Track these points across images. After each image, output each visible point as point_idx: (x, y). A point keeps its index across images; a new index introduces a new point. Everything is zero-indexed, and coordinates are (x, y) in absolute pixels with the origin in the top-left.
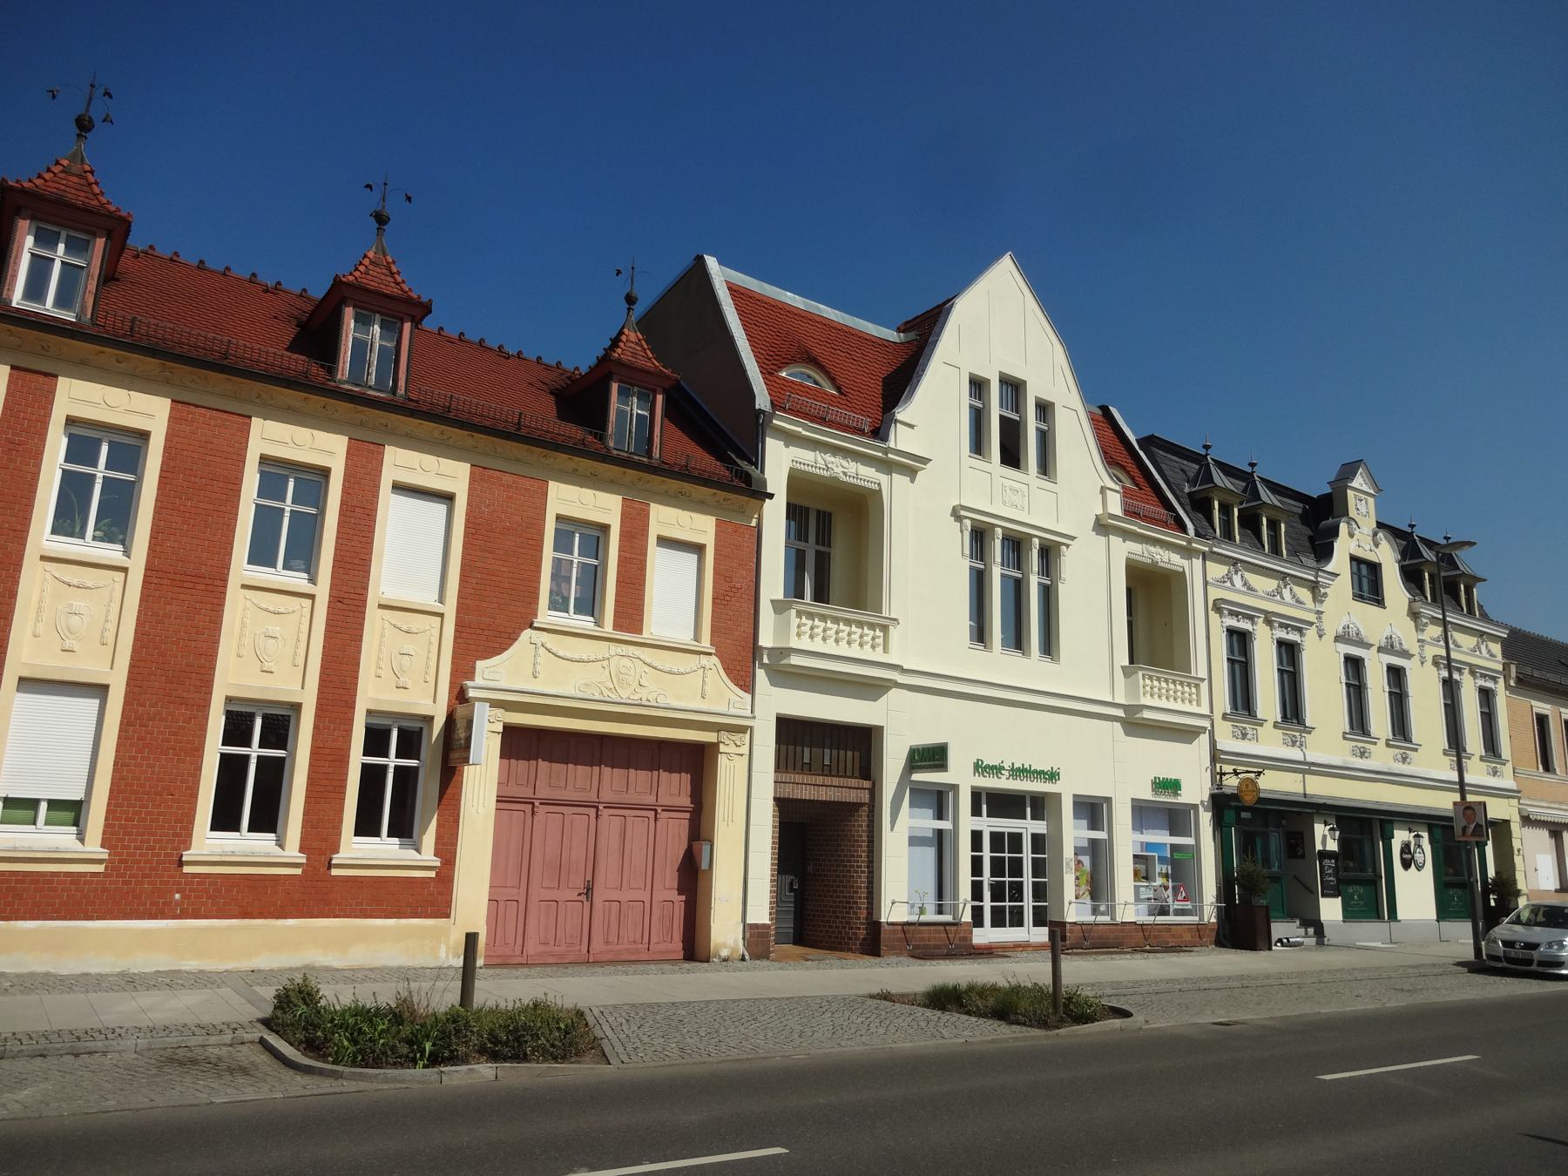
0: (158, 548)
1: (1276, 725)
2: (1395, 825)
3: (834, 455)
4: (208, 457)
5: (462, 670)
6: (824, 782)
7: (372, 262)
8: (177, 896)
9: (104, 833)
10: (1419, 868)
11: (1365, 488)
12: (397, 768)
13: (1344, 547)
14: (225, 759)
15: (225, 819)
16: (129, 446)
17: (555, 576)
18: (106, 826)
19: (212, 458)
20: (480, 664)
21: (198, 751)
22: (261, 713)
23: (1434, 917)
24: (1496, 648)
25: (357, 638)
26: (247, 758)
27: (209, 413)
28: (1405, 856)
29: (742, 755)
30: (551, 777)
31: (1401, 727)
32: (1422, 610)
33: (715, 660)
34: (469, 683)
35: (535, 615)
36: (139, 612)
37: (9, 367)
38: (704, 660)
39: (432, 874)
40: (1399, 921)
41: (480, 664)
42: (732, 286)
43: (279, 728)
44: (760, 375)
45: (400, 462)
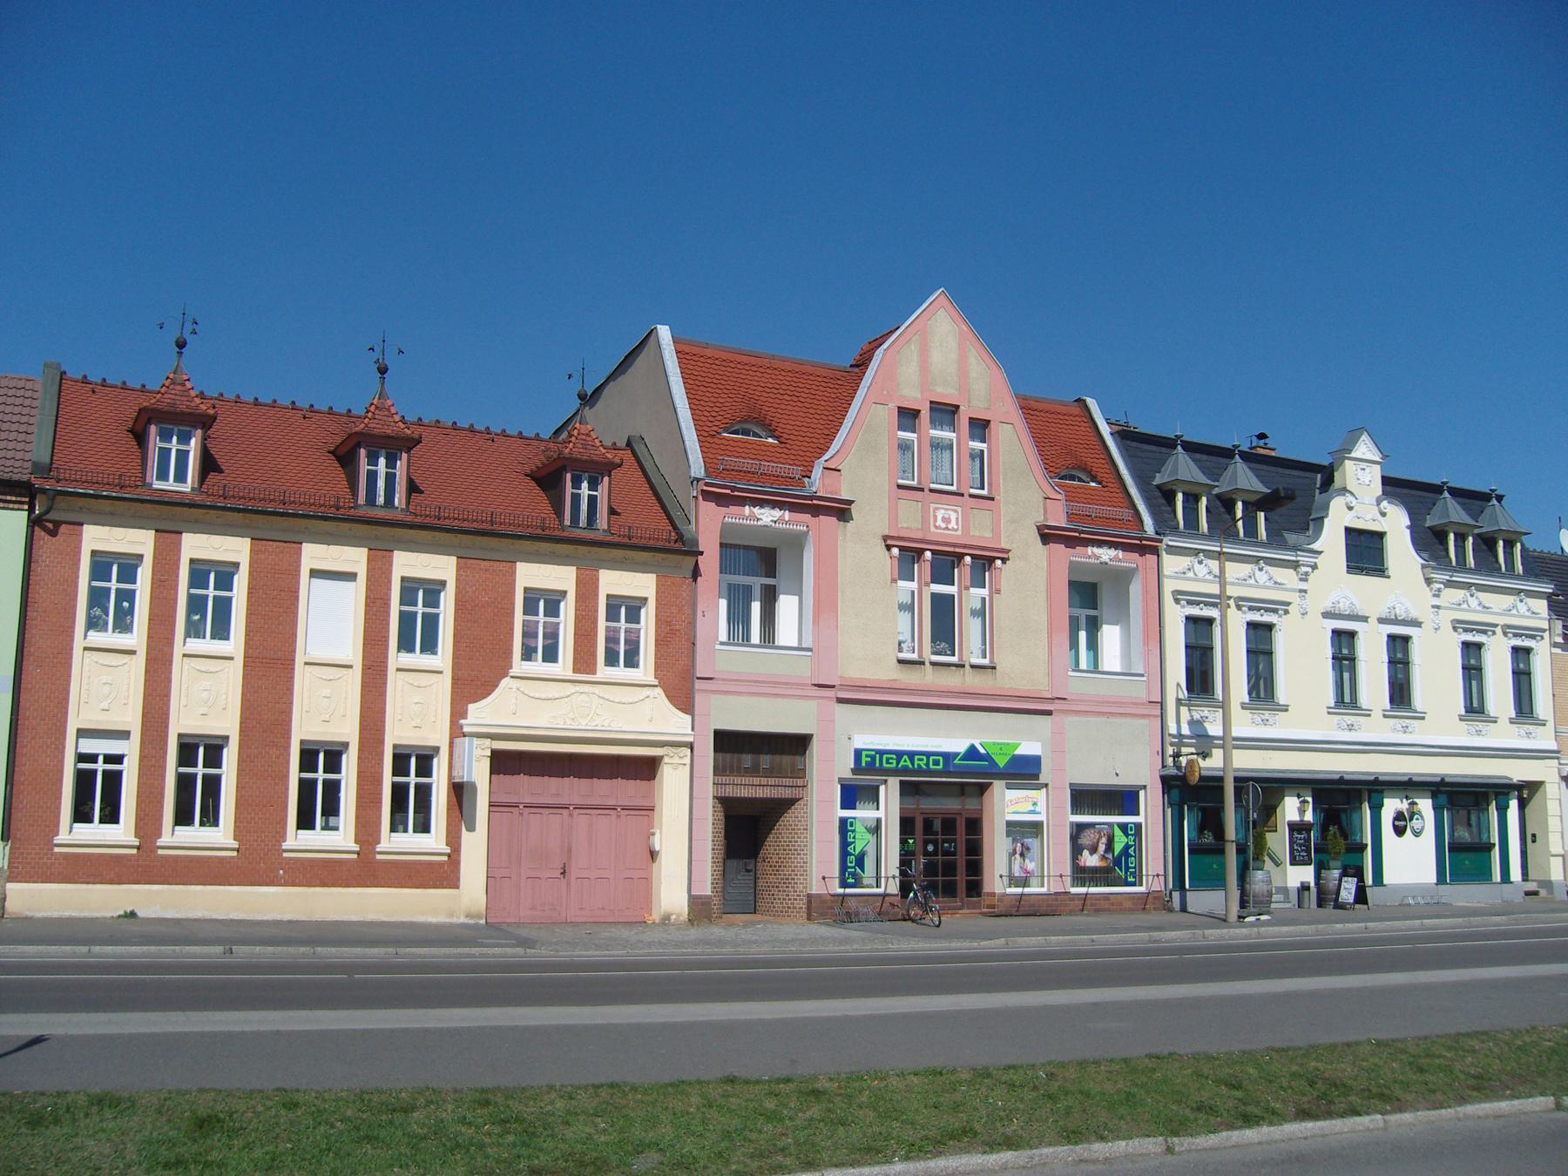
0: (251, 642)
1: (1512, 721)
2: (1385, 794)
3: (762, 507)
4: (277, 576)
5: (458, 713)
6: (768, 782)
7: (377, 408)
8: (281, 872)
9: (235, 831)
10: (1417, 834)
11: (1369, 456)
12: (105, 772)
13: (1338, 517)
14: (302, 782)
15: (305, 822)
16: (433, 590)
17: (525, 635)
18: (235, 826)
19: (280, 576)
20: (471, 707)
21: (286, 777)
22: (203, 743)
23: (1434, 880)
24: (1541, 606)
25: (383, 694)
26: (195, 775)
27: (275, 544)
28: (1397, 823)
29: (685, 765)
30: (526, 787)
31: (1400, 694)
32: (1433, 575)
33: (659, 691)
34: (462, 722)
35: (511, 667)
36: (243, 686)
37: (154, 531)
38: (647, 691)
39: (445, 858)
40: (1385, 886)
41: (471, 707)
42: (1034, 405)
43: (334, 759)
44: (697, 444)
45: (314, 555)
